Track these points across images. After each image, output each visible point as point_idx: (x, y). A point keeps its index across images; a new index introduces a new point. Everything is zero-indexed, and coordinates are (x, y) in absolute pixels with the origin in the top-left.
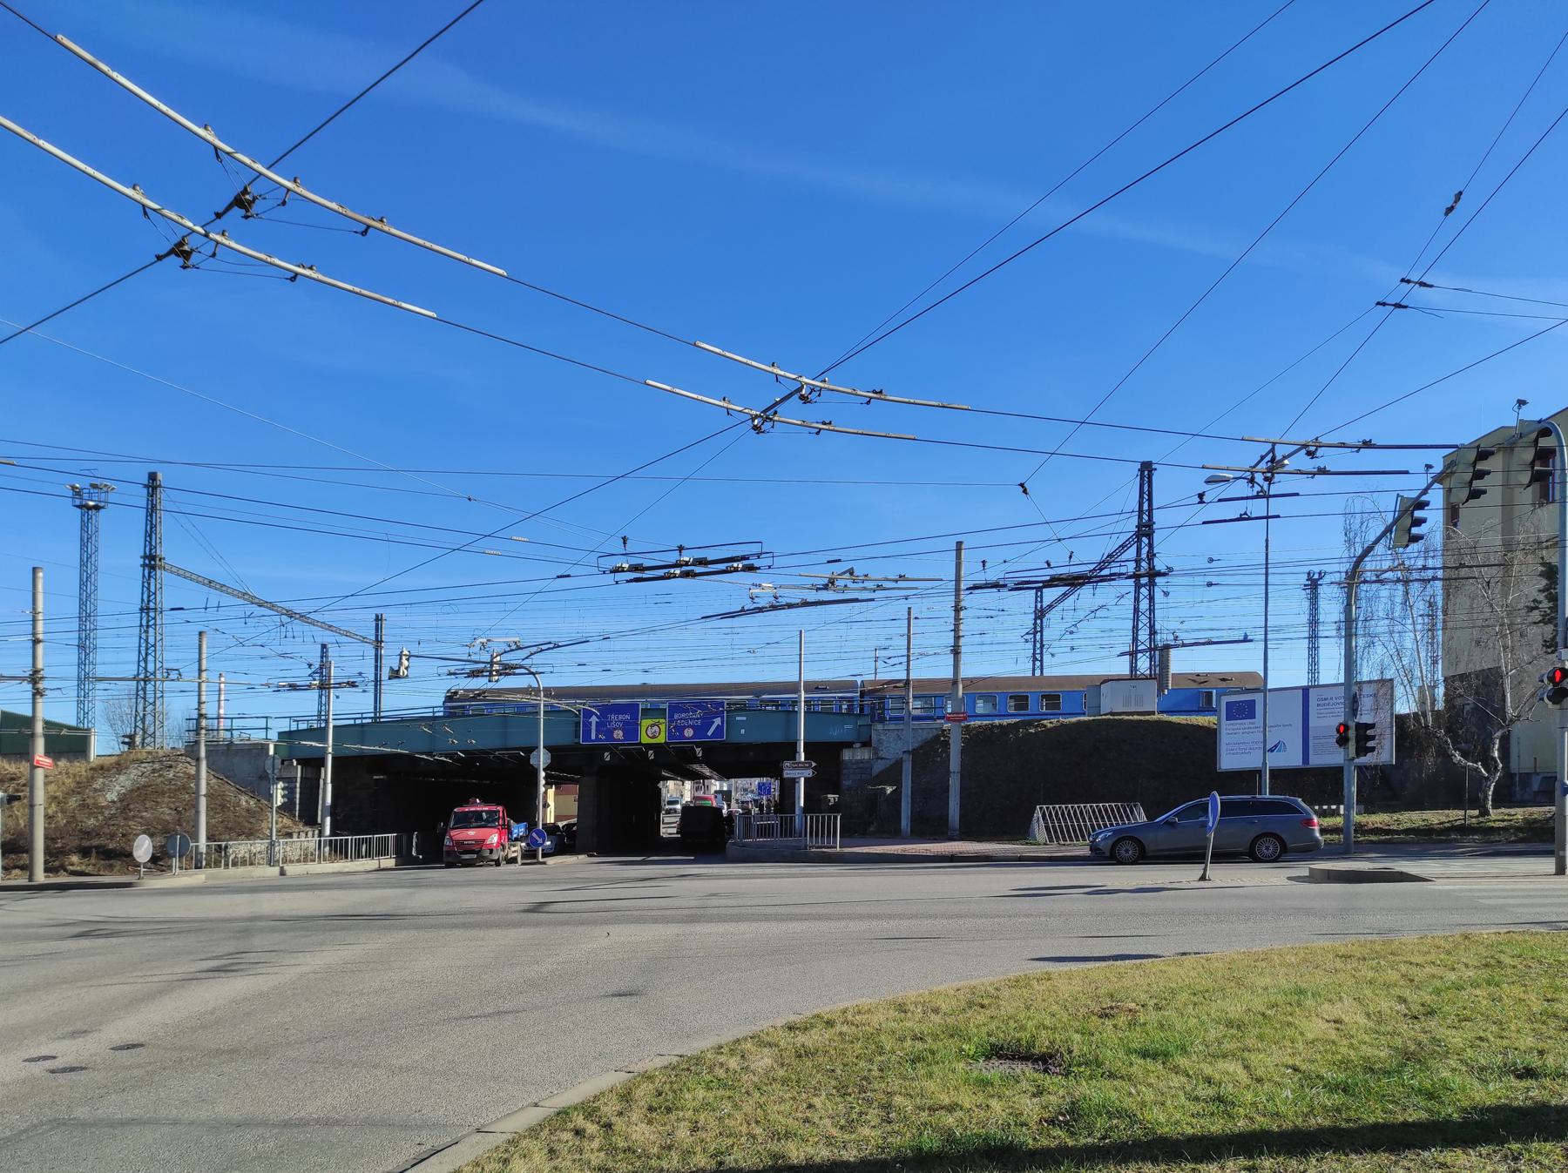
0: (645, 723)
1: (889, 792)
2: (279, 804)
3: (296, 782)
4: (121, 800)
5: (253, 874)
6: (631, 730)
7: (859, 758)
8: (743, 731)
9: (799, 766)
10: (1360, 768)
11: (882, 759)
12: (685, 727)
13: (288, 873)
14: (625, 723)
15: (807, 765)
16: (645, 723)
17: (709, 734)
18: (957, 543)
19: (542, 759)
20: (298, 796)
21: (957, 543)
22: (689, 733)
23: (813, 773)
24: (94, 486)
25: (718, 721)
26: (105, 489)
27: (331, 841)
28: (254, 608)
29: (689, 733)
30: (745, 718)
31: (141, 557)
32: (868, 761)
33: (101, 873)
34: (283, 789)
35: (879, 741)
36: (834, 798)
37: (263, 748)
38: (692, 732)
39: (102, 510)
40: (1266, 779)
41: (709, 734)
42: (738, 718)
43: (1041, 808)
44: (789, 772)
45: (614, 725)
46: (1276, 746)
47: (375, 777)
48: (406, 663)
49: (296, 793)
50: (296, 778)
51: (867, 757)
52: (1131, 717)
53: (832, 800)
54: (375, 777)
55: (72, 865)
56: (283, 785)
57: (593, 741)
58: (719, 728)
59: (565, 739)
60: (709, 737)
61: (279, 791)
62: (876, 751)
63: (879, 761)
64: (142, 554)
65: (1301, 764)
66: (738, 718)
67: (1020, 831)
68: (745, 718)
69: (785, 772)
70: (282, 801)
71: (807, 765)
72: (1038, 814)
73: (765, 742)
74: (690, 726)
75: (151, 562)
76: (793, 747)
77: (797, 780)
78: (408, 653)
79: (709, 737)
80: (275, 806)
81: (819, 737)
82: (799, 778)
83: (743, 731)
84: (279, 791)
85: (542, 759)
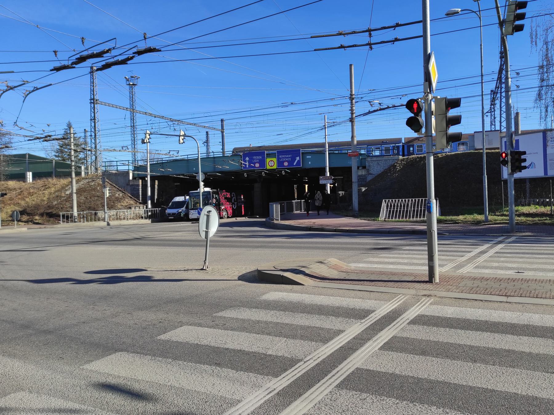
0: (268, 160)
1: (363, 190)
2: (107, 196)
3: (139, 186)
4: (69, 194)
5: (94, 225)
6: (262, 163)
7: (360, 174)
8: (310, 163)
9: (328, 179)
10: (516, 181)
11: (371, 174)
12: (284, 161)
13: (111, 224)
14: (260, 160)
15: (330, 178)
16: (268, 160)
17: (295, 164)
18: (350, 65)
19: (201, 177)
20: (140, 192)
21: (350, 65)
22: (286, 164)
23: (333, 181)
24: (132, 77)
25: (298, 158)
26: (136, 78)
27: (152, 210)
28: (153, 119)
29: (286, 164)
30: (310, 157)
31: (90, 100)
32: (365, 175)
33: (45, 223)
34: (109, 190)
35: (369, 166)
36: (342, 193)
37: (127, 173)
38: (259, 165)
39: (136, 86)
40: (485, 185)
41: (295, 164)
42: (307, 157)
43: (385, 201)
44: (322, 181)
45: (255, 161)
46: (530, 165)
47: (176, 184)
48: (148, 137)
49: (139, 191)
50: (139, 185)
51: (364, 174)
52: (493, 151)
53: (341, 194)
54: (176, 184)
55: (36, 220)
56: (109, 189)
57: (248, 168)
58: (299, 161)
59: (209, 169)
60: (294, 166)
61: (107, 191)
62: (368, 170)
63: (370, 175)
64: (90, 98)
65: (544, 175)
66: (307, 157)
67: (374, 213)
68: (310, 157)
69: (320, 181)
70: (109, 195)
71: (330, 178)
72: (384, 205)
73: (311, 167)
74: (286, 161)
75: (93, 101)
76: (324, 169)
77: (326, 185)
78: (150, 133)
79: (294, 166)
80: (106, 197)
81: (335, 165)
82: (327, 184)
83: (310, 163)
84: (107, 191)
85: (201, 177)
